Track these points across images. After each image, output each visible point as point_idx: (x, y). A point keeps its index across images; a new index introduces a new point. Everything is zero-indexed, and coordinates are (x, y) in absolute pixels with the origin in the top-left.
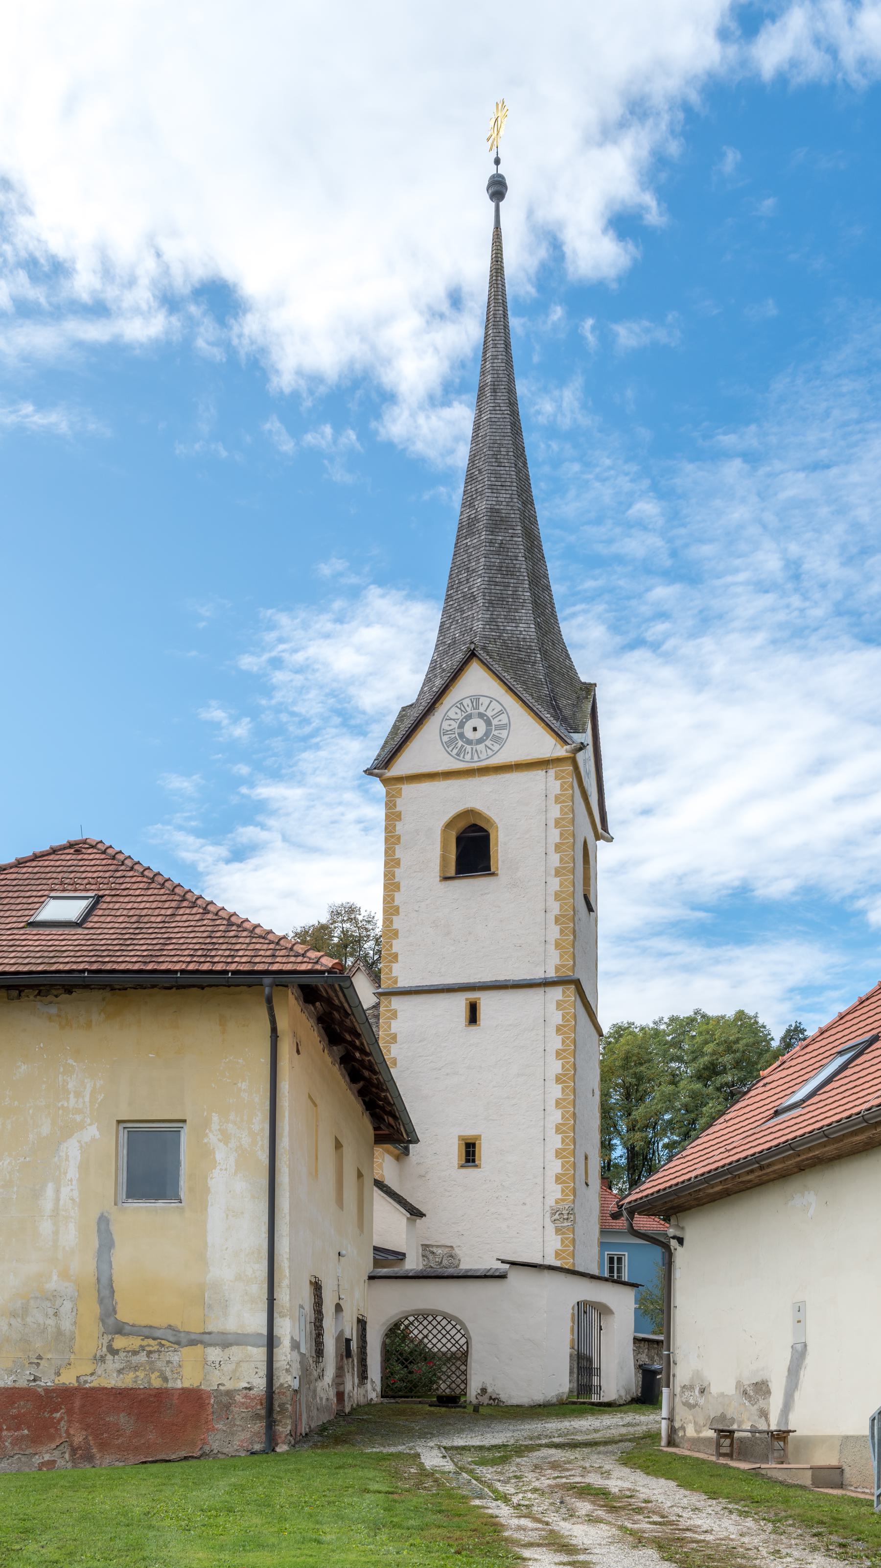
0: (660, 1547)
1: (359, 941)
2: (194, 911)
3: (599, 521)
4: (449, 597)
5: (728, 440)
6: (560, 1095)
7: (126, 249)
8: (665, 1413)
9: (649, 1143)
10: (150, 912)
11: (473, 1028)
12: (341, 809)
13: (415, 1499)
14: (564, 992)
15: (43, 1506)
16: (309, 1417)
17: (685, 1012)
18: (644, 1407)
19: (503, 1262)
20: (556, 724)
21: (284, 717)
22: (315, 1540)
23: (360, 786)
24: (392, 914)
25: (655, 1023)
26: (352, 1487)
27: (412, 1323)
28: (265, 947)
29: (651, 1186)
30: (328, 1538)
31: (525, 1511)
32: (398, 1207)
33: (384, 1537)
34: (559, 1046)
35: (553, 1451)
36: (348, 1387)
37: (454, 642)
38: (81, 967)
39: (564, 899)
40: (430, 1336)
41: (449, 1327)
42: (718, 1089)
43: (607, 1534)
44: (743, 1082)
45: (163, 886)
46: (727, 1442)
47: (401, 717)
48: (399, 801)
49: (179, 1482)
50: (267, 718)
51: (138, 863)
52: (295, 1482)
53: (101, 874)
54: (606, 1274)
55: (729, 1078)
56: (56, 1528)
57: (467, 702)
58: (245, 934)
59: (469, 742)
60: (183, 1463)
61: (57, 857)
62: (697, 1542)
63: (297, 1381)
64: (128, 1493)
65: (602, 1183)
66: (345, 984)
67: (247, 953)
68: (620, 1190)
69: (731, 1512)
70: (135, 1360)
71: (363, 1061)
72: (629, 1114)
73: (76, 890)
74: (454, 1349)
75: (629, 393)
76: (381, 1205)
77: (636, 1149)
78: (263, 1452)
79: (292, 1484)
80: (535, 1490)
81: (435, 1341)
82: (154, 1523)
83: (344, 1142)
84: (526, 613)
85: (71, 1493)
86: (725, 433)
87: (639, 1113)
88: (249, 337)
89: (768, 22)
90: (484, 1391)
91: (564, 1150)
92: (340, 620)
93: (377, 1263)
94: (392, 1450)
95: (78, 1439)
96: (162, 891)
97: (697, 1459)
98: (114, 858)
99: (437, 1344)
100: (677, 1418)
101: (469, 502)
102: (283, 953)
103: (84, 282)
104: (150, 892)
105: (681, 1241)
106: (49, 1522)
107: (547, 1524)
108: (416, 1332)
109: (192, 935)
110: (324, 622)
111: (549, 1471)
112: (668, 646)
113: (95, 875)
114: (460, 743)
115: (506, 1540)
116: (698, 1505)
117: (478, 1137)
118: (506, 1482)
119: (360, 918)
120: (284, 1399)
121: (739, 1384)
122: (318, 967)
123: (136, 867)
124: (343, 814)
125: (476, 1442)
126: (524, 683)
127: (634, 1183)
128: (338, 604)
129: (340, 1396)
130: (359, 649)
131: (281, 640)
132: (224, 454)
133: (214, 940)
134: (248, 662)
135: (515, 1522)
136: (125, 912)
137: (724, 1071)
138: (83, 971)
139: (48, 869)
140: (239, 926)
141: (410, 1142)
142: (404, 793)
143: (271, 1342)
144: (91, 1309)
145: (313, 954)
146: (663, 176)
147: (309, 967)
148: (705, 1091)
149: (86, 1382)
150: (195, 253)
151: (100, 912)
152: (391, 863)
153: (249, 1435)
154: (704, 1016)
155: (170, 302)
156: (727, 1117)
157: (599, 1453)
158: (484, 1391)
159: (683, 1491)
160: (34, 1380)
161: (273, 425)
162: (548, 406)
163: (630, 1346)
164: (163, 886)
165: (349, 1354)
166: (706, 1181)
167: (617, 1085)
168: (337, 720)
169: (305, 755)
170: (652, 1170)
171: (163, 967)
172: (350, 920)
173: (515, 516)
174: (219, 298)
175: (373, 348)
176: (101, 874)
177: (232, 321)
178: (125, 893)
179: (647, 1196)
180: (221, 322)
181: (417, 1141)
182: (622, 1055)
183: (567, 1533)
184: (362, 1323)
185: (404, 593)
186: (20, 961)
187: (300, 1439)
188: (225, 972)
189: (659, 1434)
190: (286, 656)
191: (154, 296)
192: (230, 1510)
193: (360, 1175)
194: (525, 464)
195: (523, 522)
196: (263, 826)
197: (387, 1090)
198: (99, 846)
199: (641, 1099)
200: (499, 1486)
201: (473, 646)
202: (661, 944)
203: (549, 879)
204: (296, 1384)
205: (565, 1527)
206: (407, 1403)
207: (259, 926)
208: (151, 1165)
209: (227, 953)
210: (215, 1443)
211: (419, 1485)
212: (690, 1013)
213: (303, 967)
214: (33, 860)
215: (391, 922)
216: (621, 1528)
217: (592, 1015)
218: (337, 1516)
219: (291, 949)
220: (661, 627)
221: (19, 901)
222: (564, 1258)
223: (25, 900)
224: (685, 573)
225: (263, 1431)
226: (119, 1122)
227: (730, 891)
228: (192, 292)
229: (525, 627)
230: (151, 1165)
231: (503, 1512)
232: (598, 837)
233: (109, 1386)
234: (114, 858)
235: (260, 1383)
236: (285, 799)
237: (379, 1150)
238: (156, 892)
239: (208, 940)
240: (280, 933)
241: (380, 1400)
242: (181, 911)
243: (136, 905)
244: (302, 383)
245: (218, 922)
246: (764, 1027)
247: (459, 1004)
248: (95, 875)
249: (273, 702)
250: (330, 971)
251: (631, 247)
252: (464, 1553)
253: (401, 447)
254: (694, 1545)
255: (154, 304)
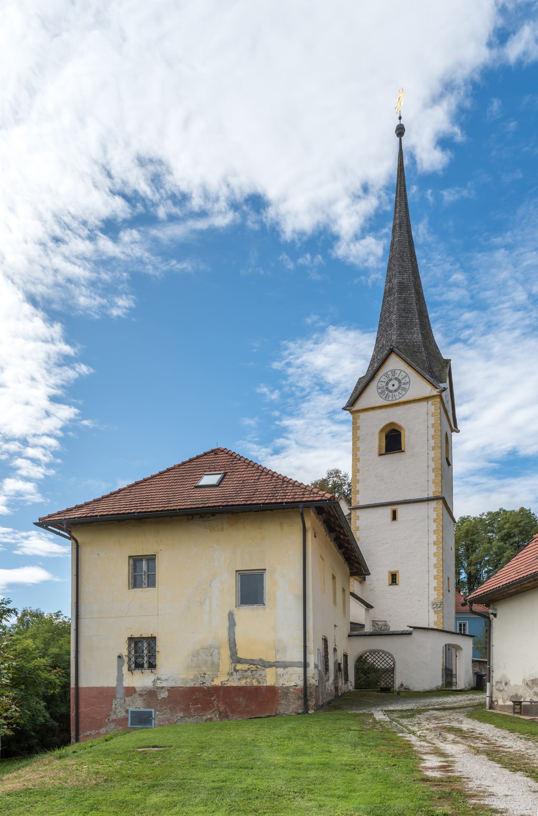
0: (488, 755)
1: (341, 486)
2: (268, 476)
3: (435, 286)
4: (380, 325)
5: (497, 240)
6: (436, 551)
7: (214, 184)
8: (488, 694)
9: (478, 571)
10: (248, 478)
11: (395, 522)
12: (321, 428)
13: (372, 733)
14: (437, 503)
15: (209, 737)
16: (323, 698)
17: (495, 510)
18: (477, 692)
19: (410, 627)
20: (432, 380)
21: (294, 389)
22: (328, 751)
23: (329, 417)
24: (356, 473)
25: (480, 515)
26: (343, 728)
27: (368, 656)
28: (300, 490)
29: (480, 591)
30: (334, 750)
31: (423, 739)
32: (361, 604)
33: (359, 750)
34: (435, 528)
35: (435, 712)
36: (340, 684)
37: (383, 346)
38: (219, 504)
39: (437, 460)
40: (377, 661)
41: (385, 657)
42: (512, 545)
43: (462, 749)
44: (523, 540)
45: (253, 466)
46: (519, 707)
47: (359, 383)
48: (358, 421)
49: (266, 726)
50: (286, 389)
51: (242, 457)
52: (316, 727)
53: (226, 463)
54: (458, 632)
55: (517, 539)
56: (215, 746)
57: (389, 373)
58: (290, 485)
59: (391, 391)
60: (268, 718)
61: (207, 457)
62: (506, 752)
63: (317, 682)
64: (244, 731)
65: (456, 591)
66: (335, 505)
67: (292, 494)
68: (464, 593)
69: (521, 739)
70: (245, 674)
71: (344, 539)
72: (468, 558)
73: (215, 471)
74: (388, 667)
75: (451, 223)
76: (354, 604)
77: (472, 574)
78: (303, 713)
79: (316, 727)
80: (427, 729)
81: (379, 663)
82: (257, 744)
83: (336, 576)
84: (417, 329)
85: (220, 732)
86: (495, 238)
87: (473, 557)
88: (271, 218)
89: (512, 35)
90: (402, 685)
91: (438, 575)
92: (316, 343)
93: (352, 629)
94: (361, 712)
95: (222, 709)
96: (253, 469)
97: (504, 715)
98: (231, 455)
99: (380, 664)
100: (494, 696)
101: (389, 280)
102: (308, 493)
103: (196, 203)
104: (248, 470)
105: (495, 615)
106: (212, 744)
107: (434, 744)
108: (370, 659)
109: (267, 487)
110: (310, 345)
111: (433, 721)
112: (471, 341)
113: (224, 463)
114: (387, 392)
115: (415, 751)
116: (505, 735)
117: (397, 571)
118: (413, 726)
119: (341, 475)
120: (312, 690)
121: (524, 680)
122: (324, 498)
123: (241, 459)
124: (322, 430)
125: (399, 708)
126: (416, 362)
127: (471, 590)
128: (315, 336)
129: (336, 688)
130: (326, 355)
131: (290, 354)
132: (262, 272)
133: (277, 489)
134: (276, 365)
135: (419, 743)
136: (237, 479)
137: (515, 536)
138: (220, 506)
139: (203, 462)
140: (287, 482)
141: (366, 575)
142: (361, 417)
143: (305, 665)
144: (226, 653)
145: (321, 493)
146: (463, 118)
147: (320, 498)
148: (506, 546)
149: (225, 684)
150: (243, 184)
151: (226, 480)
152: (355, 450)
153: (296, 706)
154: (504, 511)
155: (234, 206)
156: (517, 557)
157: (457, 712)
158: (402, 685)
159: (497, 729)
160: (203, 684)
161: (284, 257)
162: (420, 231)
163: (471, 664)
164: (253, 466)
165: (340, 670)
166: (508, 587)
167: (462, 545)
168: (317, 388)
169: (303, 405)
170: (480, 583)
171: (255, 502)
172: (337, 476)
173: (411, 284)
174: (257, 202)
175: (328, 216)
176: (226, 463)
177: (263, 211)
178: (237, 471)
179: (478, 595)
180: (258, 212)
181: (369, 574)
182: (465, 531)
183: (443, 748)
184: (345, 656)
185: (345, 328)
186: (192, 503)
187: (319, 708)
188: (282, 503)
189: (485, 704)
190: (292, 361)
191: (228, 204)
192: (290, 738)
193: (344, 590)
194: (415, 259)
195: (414, 287)
196: (287, 438)
197: (356, 552)
198: (225, 451)
199: (474, 551)
200: (410, 727)
201: (392, 347)
202: (475, 479)
203: (429, 452)
204: (317, 684)
205: (442, 746)
206: (367, 691)
207: (296, 481)
208: (251, 589)
209: (283, 494)
210: (281, 709)
211: (373, 727)
212: (497, 510)
213: (317, 499)
214: (196, 459)
215: (356, 476)
216: (469, 746)
217: (450, 512)
218: (337, 741)
219: (311, 491)
220: (468, 332)
221: (191, 477)
222: (439, 625)
223: (193, 477)
224: (479, 306)
225: (302, 704)
226: (237, 571)
227: (507, 453)
228: (245, 200)
229: (417, 336)
230: (251, 589)
231: (413, 739)
232: (452, 431)
233: (235, 686)
234: (231, 455)
235: (301, 683)
236: (296, 425)
237: (352, 579)
238: (250, 469)
239: (274, 489)
240: (306, 484)
241: (354, 690)
242: (262, 477)
243: (242, 476)
244: (296, 236)
245: (278, 481)
246: (534, 514)
247: (388, 511)
248: (224, 463)
249: (288, 382)
250: (329, 500)
251: (449, 153)
252: (396, 757)
253: (343, 260)
254: (504, 754)
255: (228, 208)
